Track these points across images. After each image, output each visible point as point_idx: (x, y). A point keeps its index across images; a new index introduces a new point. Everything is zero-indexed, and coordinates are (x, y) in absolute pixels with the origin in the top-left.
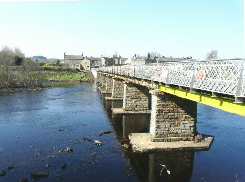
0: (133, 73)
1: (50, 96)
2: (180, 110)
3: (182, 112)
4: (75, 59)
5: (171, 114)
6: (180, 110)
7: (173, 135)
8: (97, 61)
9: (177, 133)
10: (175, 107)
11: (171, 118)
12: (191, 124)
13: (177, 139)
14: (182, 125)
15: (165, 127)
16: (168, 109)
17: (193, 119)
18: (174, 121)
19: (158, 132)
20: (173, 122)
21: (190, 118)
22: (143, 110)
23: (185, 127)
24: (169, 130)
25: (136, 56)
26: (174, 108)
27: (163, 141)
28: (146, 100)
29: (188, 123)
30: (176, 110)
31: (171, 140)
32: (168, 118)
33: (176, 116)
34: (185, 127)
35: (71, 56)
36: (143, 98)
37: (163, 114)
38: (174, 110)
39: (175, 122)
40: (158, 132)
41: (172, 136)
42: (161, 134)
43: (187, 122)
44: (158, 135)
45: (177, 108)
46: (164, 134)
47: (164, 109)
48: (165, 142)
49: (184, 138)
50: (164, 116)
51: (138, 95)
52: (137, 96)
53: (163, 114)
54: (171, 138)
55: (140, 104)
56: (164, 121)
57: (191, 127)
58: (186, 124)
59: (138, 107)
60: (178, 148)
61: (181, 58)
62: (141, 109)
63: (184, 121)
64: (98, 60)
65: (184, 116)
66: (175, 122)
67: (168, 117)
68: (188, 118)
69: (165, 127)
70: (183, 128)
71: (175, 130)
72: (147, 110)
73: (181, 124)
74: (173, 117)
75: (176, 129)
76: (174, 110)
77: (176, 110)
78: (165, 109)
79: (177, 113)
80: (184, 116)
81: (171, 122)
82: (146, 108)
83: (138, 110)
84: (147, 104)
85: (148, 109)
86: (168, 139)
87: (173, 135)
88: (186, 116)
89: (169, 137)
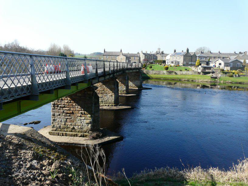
0: (116, 68)
1: (219, 92)
2: (76, 105)
3: (78, 108)
4: (114, 55)
5: (67, 109)
6: (76, 105)
7: (69, 130)
8: (135, 57)
9: (74, 128)
10: (70, 102)
11: (67, 113)
12: (88, 121)
13: (72, 134)
14: (79, 121)
15: (61, 121)
16: (63, 104)
17: (90, 115)
18: (70, 116)
19: (54, 126)
20: (69, 117)
21: (87, 114)
22: (109, 106)
23: (81, 123)
24: (65, 124)
25: (175, 51)
26: (69, 103)
27: (59, 135)
28: (112, 96)
29: (85, 119)
30: (71, 105)
31: (66, 135)
32: (64, 113)
33: (71, 111)
34: (81, 123)
35: (110, 52)
36: (109, 94)
37: (59, 108)
38: (69, 105)
39: (71, 117)
40: (54, 126)
41: (68, 131)
42: (57, 128)
43: (83, 118)
44: (55, 129)
45: (72, 103)
46: (60, 128)
47: (58, 103)
48: (60, 135)
49: (80, 134)
50: (60, 110)
51: (103, 90)
52: (103, 91)
53: (59, 108)
54: (67, 133)
55: (106, 100)
56: (59, 115)
57: (88, 124)
58: (83, 120)
59: (104, 102)
60: (61, 143)
61: (232, 54)
62: (107, 105)
63: (81, 116)
64: (136, 56)
65: (80, 112)
66: (71, 117)
67: (64, 111)
68: (84, 114)
69: (61, 121)
70: (79, 124)
71: (71, 125)
72: (112, 106)
73: (78, 120)
74: (69, 112)
75: (72, 124)
76: (69, 105)
77: (71, 105)
78: (60, 103)
79: (73, 108)
80: (80, 112)
81: (67, 117)
82: (112, 104)
83: (103, 106)
84: (113, 100)
85: (113, 105)
86: (63, 133)
87: (69, 130)
88: (82, 112)
89: (66, 131)
